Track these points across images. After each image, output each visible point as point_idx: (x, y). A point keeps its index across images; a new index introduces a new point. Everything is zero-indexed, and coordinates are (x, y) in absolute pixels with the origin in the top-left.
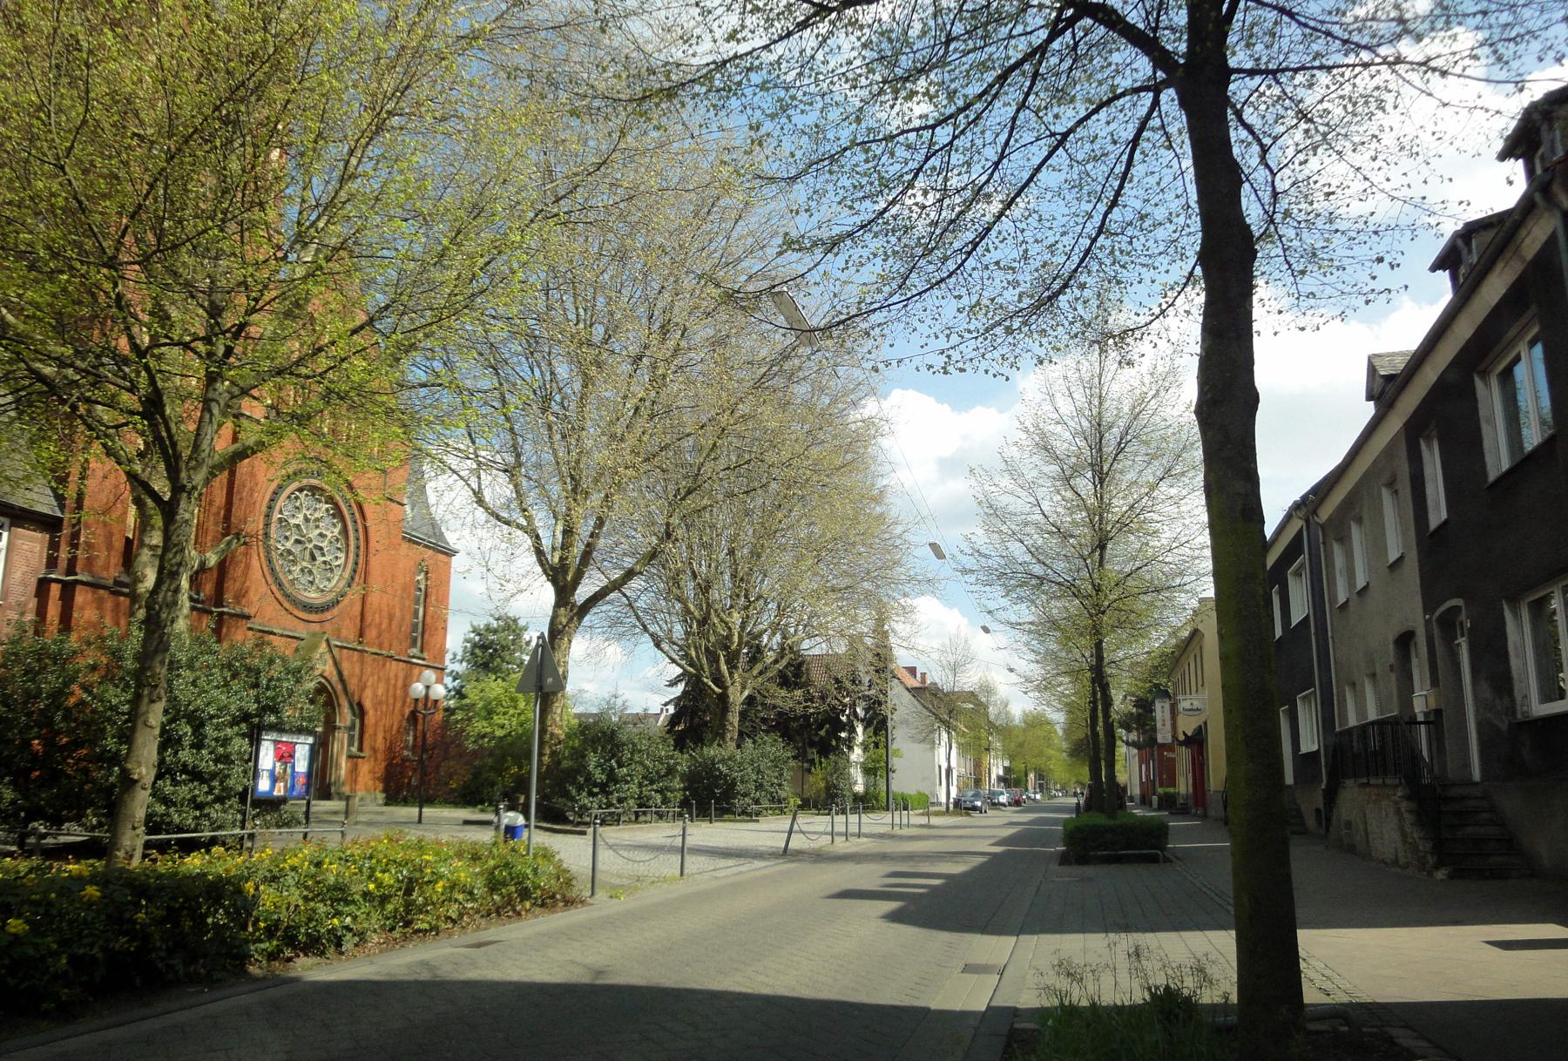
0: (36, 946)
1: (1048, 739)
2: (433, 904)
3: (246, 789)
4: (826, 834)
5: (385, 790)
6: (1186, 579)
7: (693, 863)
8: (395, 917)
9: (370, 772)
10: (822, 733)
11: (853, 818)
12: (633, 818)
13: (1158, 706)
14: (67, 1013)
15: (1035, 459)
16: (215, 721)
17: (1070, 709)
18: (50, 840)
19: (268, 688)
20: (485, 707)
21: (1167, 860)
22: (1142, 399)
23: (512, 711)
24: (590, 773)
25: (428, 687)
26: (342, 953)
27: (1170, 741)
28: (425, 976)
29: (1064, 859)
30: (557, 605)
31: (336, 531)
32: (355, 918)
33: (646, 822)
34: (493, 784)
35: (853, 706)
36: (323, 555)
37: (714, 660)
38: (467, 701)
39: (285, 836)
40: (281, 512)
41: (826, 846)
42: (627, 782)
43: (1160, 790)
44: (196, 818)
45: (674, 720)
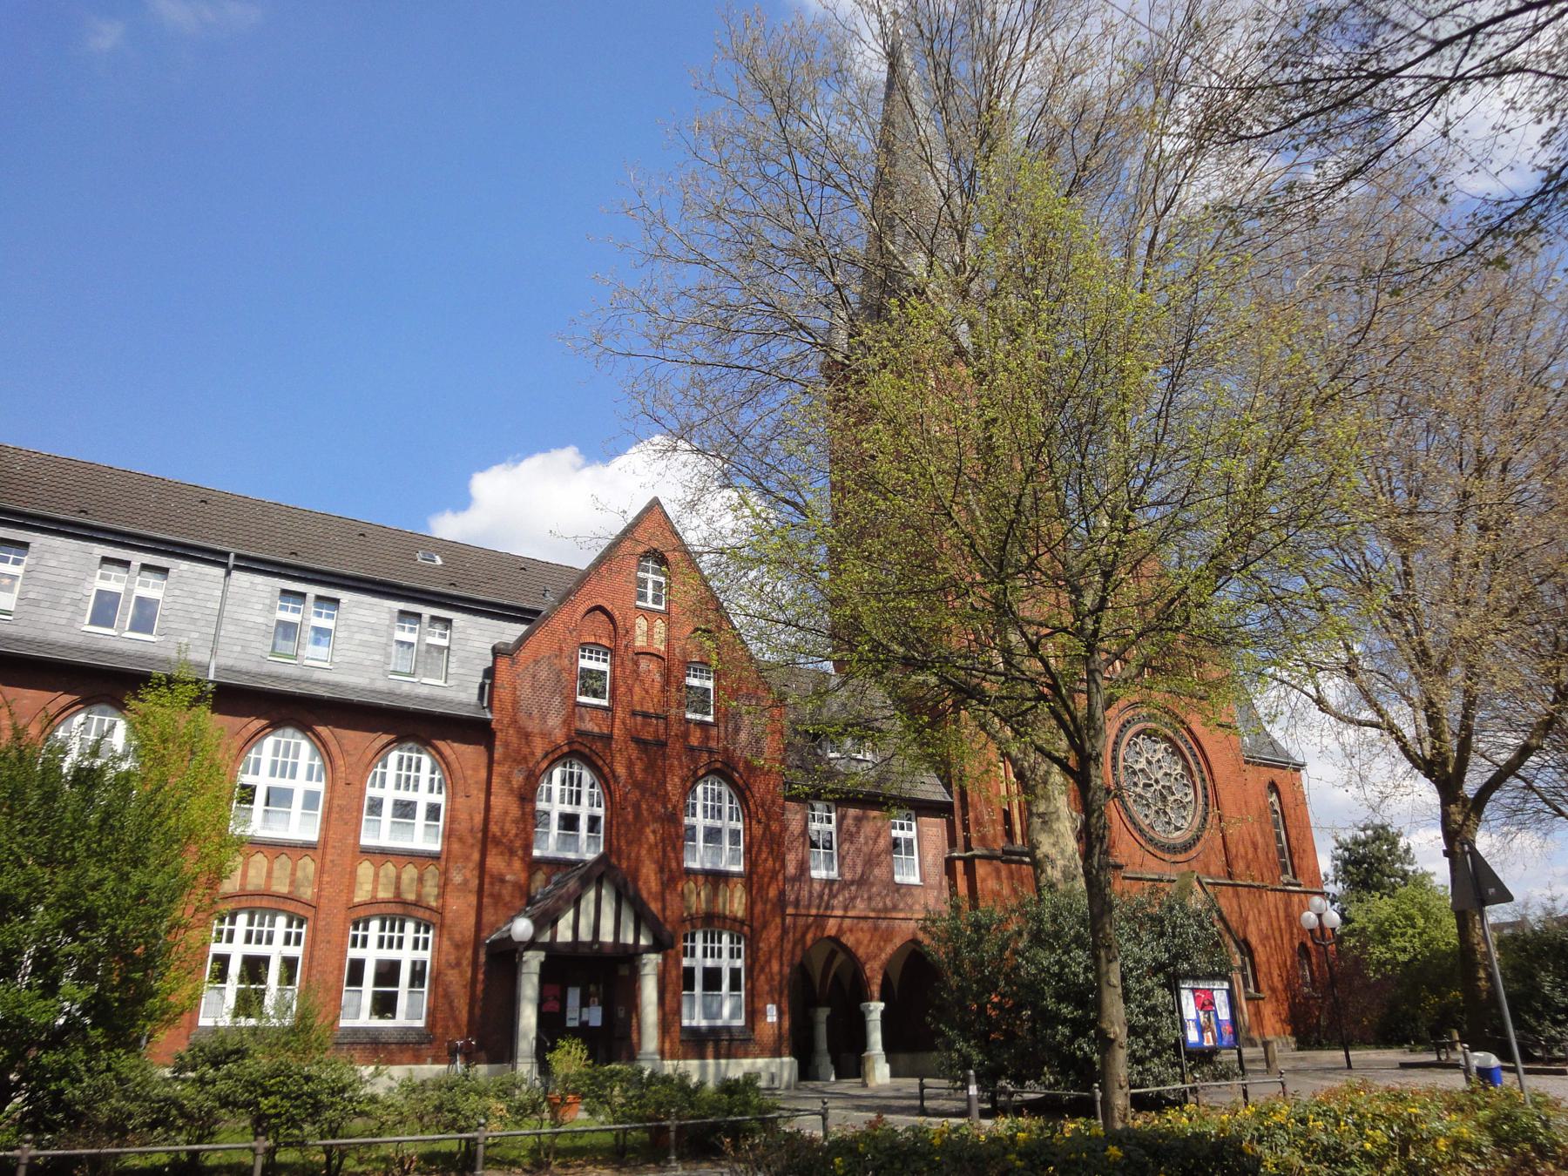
5: (1293, 1033)
18: (1017, 1098)
20: (1377, 930)
23: (1410, 932)
25: (1319, 916)
30: (1445, 803)
31: (1179, 768)
36: (1173, 794)
40: (1125, 760)
44: (1139, 1073)
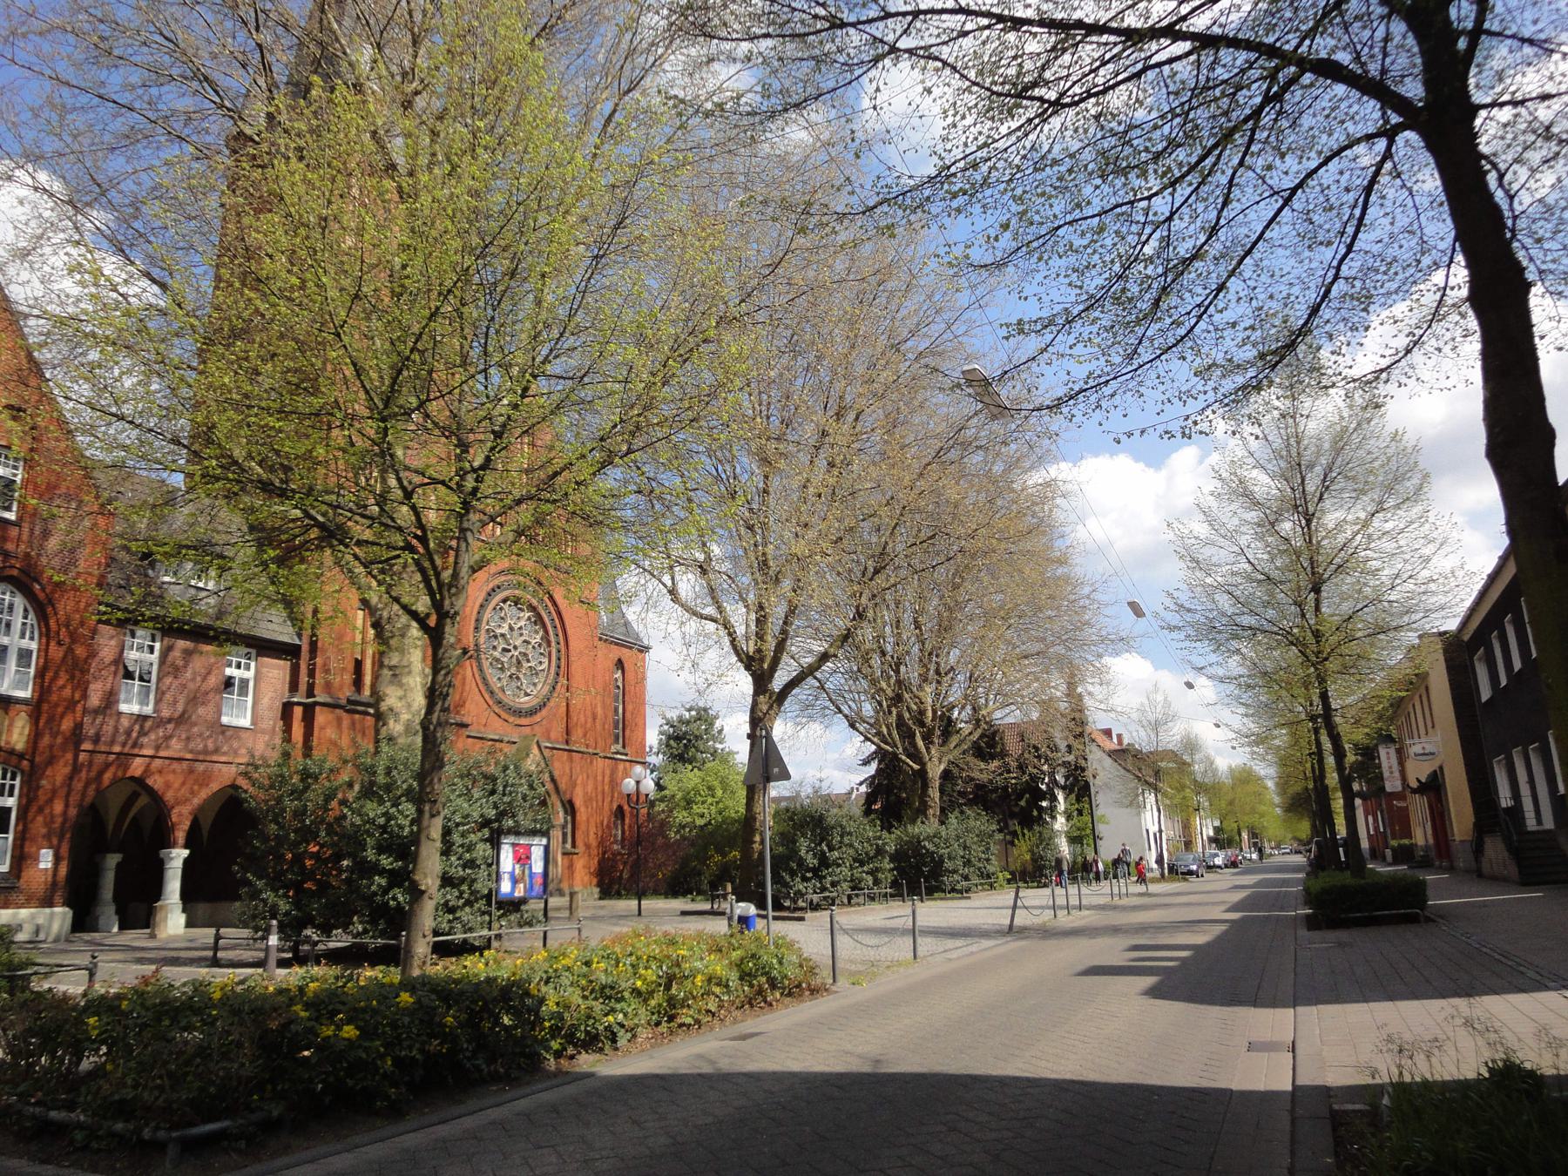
0: (366, 1049)
1: (1259, 795)
2: (694, 998)
3: (490, 891)
4: (1048, 908)
5: (599, 885)
6: (1415, 617)
7: (925, 944)
8: (659, 1012)
9: (584, 867)
10: (1023, 803)
11: (1073, 890)
12: (846, 901)
13: (1382, 751)
14: (395, 1112)
15: (1234, 506)
16: (461, 828)
17: (1283, 762)
18: (321, 947)
19: (504, 795)
20: (684, 798)
21: (1428, 920)
22: (1345, 430)
24: (801, 858)
25: (638, 783)
26: (616, 1049)
27: (1400, 789)
28: (706, 1069)
29: (1312, 923)
31: (538, 638)
32: (625, 1015)
33: (859, 905)
34: (700, 874)
35: (1052, 774)
36: (528, 661)
37: (908, 735)
38: (666, 792)
39: (526, 935)
41: (1050, 920)
42: (839, 865)
43: (1394, 843)
44: (449, 921)
45: (870, 799)
